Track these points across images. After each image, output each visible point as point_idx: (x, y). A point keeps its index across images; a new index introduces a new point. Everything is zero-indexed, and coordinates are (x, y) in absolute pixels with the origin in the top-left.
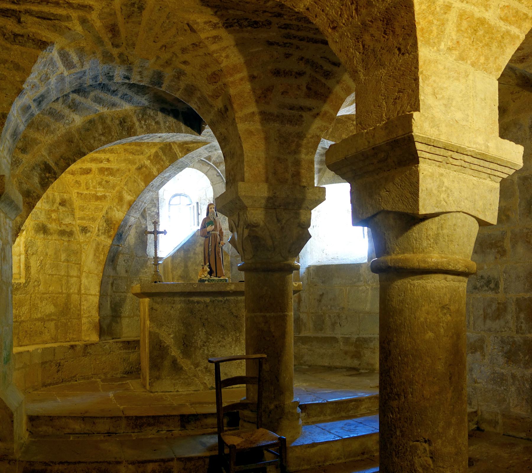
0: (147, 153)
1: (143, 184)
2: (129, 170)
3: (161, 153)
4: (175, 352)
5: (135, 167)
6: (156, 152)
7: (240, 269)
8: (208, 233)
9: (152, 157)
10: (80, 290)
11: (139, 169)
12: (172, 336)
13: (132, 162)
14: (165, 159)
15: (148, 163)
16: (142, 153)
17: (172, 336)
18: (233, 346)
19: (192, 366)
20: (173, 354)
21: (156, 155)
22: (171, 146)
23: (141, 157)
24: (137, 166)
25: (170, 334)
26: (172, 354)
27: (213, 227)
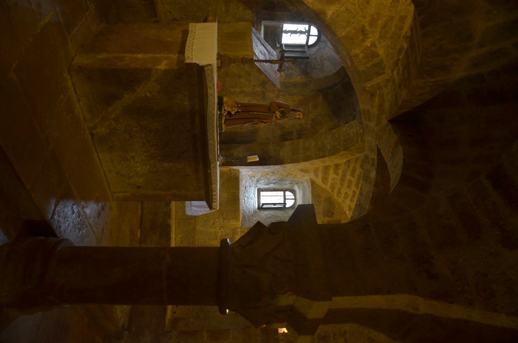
0: (380, 44)
1: (343, 34)
2: (364, 17)
3: (376, 60)
4: (128, 98)
5: (367, 25)
6: (378, 55)
7: (224, 242)
8: (274, 112)
9: (373, 49)
10: (86, 216)
11: (363, 31)
12: (148, 94)
13: (373, 23)
14: (368, 65)
15: (368, 43)
16: (381, 38)
17: (148, 94)
18: (145, 154)
19: (114, 116)
20: (126, 96)
21: (375, 55)
22: (381, 75)
23: (377, 35)
24: (367, 28)
25: (150, 92)
26: (125, 95)
27: (279, 118)
